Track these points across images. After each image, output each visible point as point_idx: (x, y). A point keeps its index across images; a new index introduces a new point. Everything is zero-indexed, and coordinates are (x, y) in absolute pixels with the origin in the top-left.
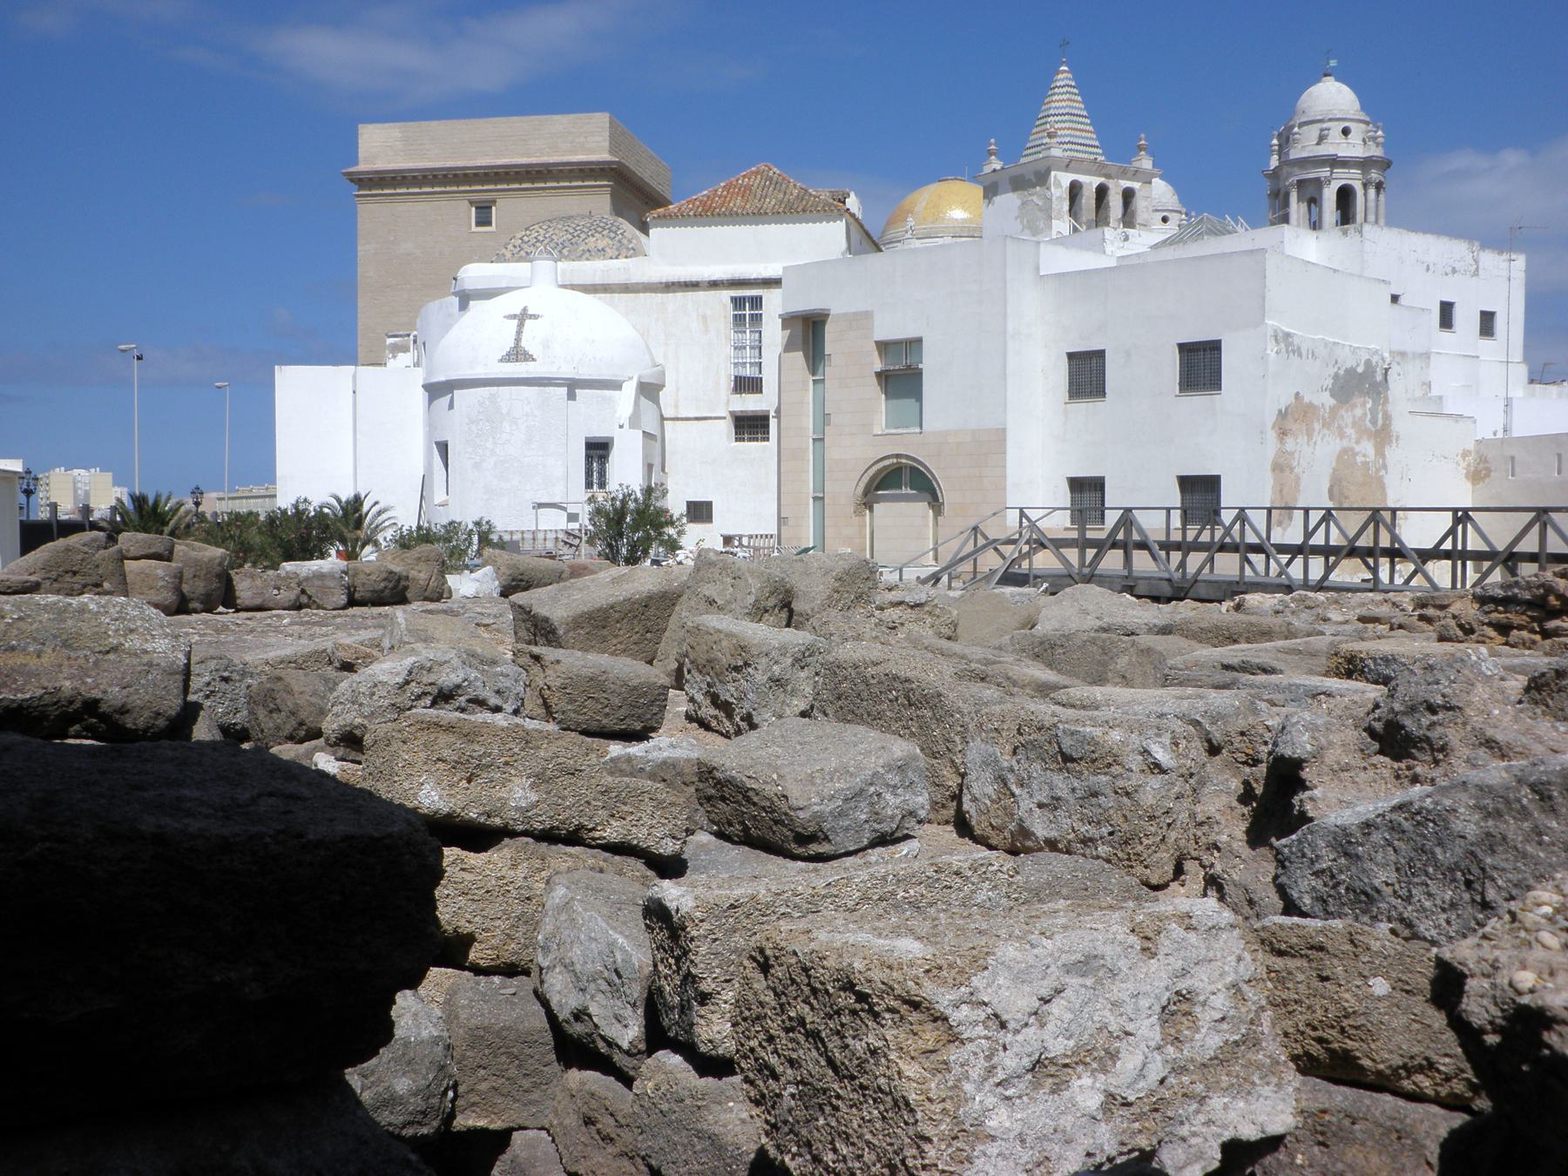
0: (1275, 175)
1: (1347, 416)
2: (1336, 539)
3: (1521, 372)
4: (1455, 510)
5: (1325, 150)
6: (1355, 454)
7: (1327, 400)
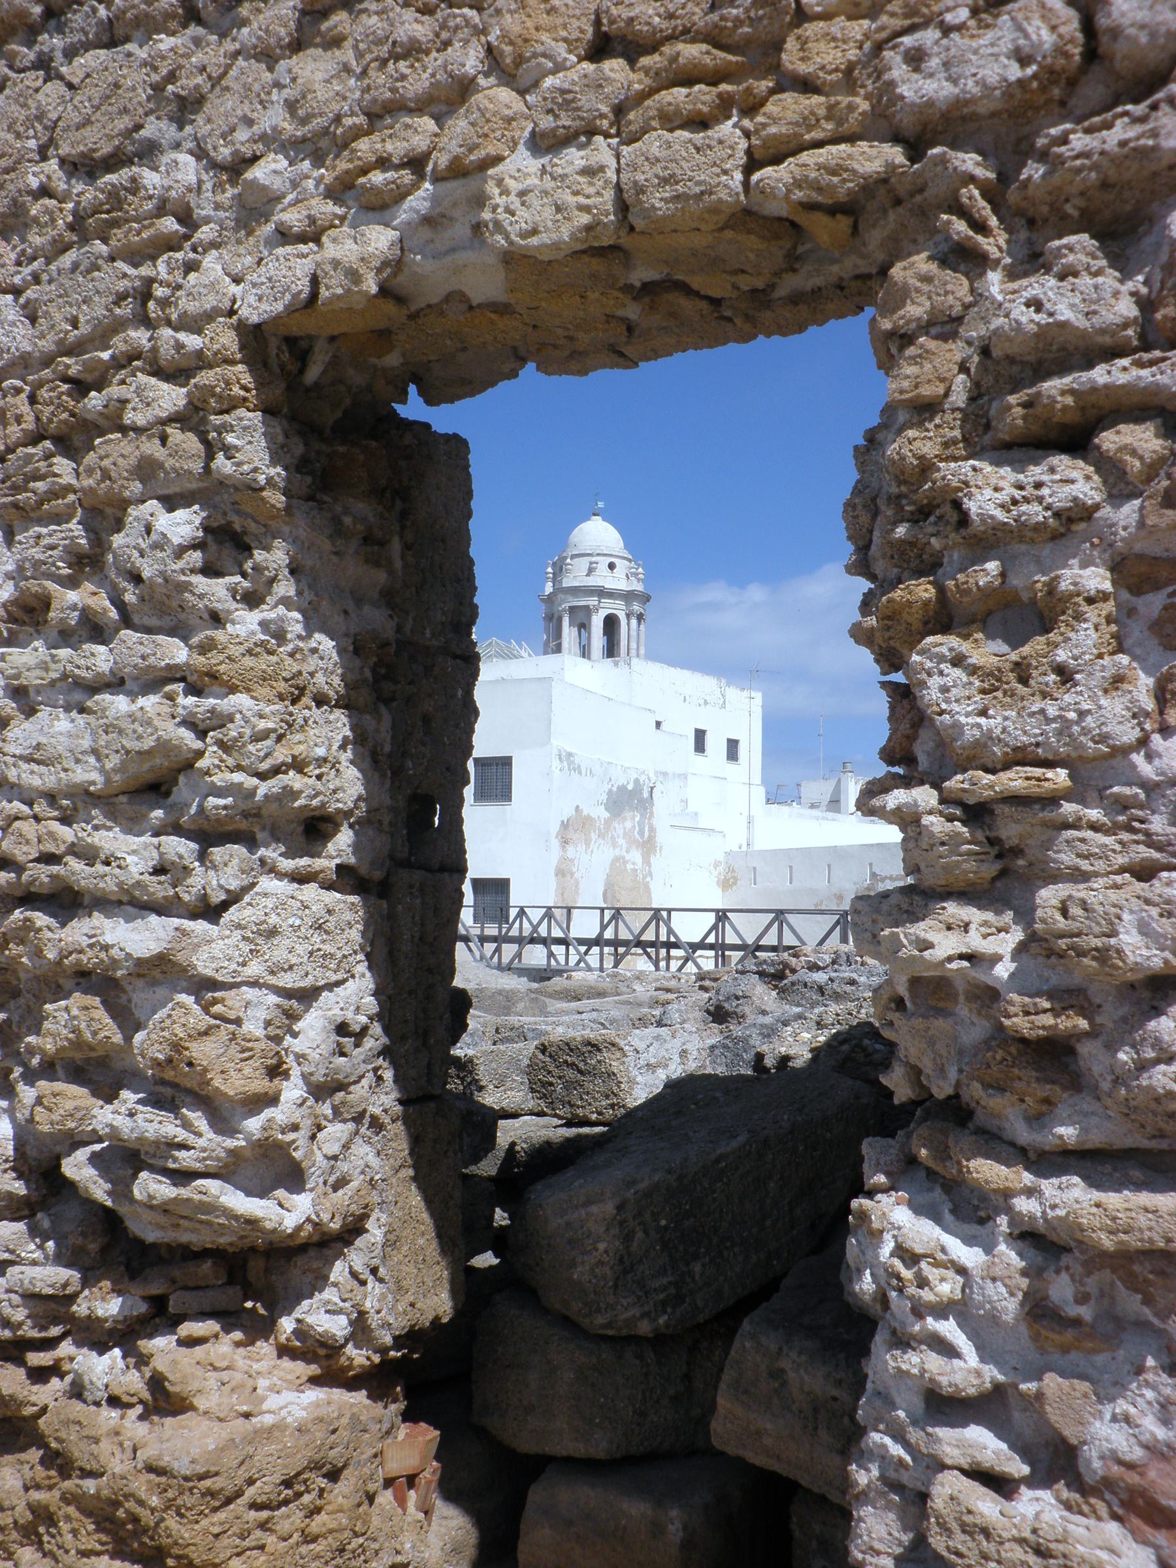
0: (550, 600)
1: (619, 828)
2: (624, 935)
3: (760, 793)
4: (717, 911)
5: (592, 581)
6: (625, 862)
7: (602, 813)
